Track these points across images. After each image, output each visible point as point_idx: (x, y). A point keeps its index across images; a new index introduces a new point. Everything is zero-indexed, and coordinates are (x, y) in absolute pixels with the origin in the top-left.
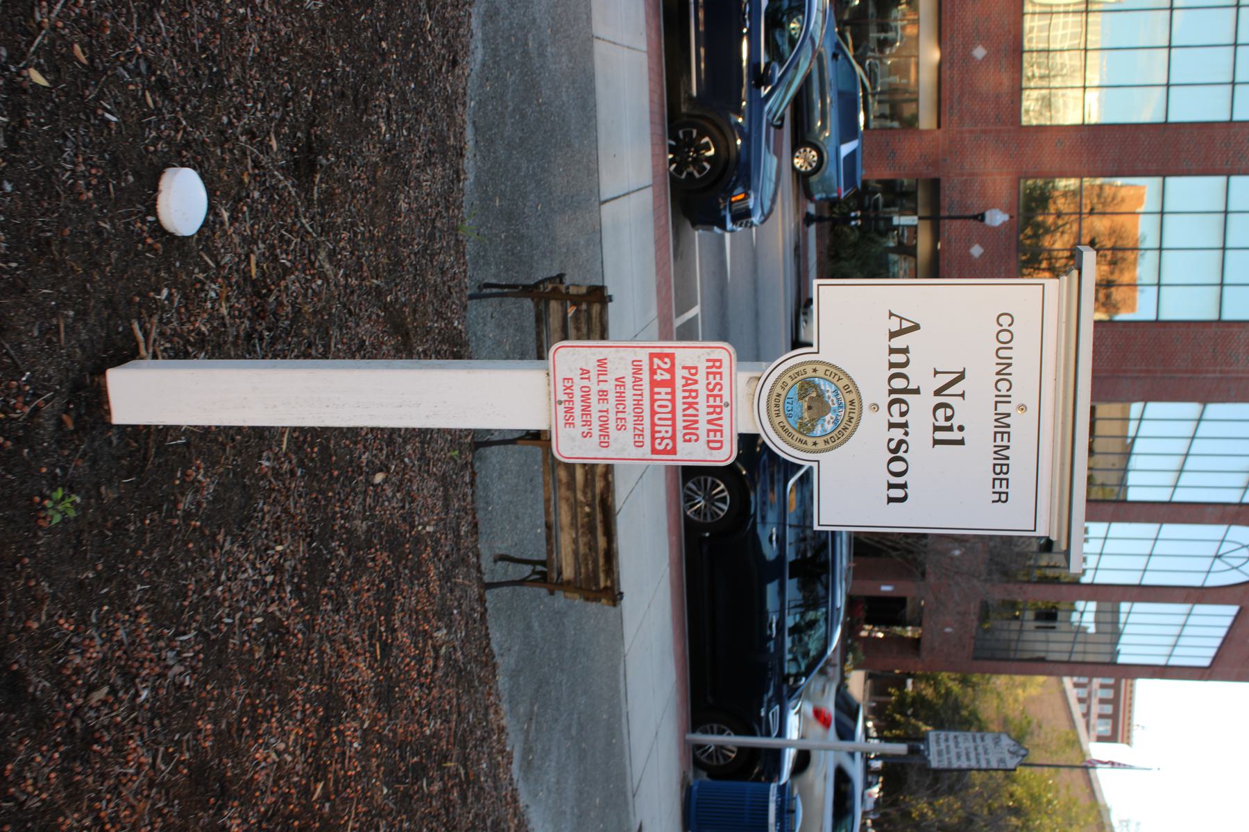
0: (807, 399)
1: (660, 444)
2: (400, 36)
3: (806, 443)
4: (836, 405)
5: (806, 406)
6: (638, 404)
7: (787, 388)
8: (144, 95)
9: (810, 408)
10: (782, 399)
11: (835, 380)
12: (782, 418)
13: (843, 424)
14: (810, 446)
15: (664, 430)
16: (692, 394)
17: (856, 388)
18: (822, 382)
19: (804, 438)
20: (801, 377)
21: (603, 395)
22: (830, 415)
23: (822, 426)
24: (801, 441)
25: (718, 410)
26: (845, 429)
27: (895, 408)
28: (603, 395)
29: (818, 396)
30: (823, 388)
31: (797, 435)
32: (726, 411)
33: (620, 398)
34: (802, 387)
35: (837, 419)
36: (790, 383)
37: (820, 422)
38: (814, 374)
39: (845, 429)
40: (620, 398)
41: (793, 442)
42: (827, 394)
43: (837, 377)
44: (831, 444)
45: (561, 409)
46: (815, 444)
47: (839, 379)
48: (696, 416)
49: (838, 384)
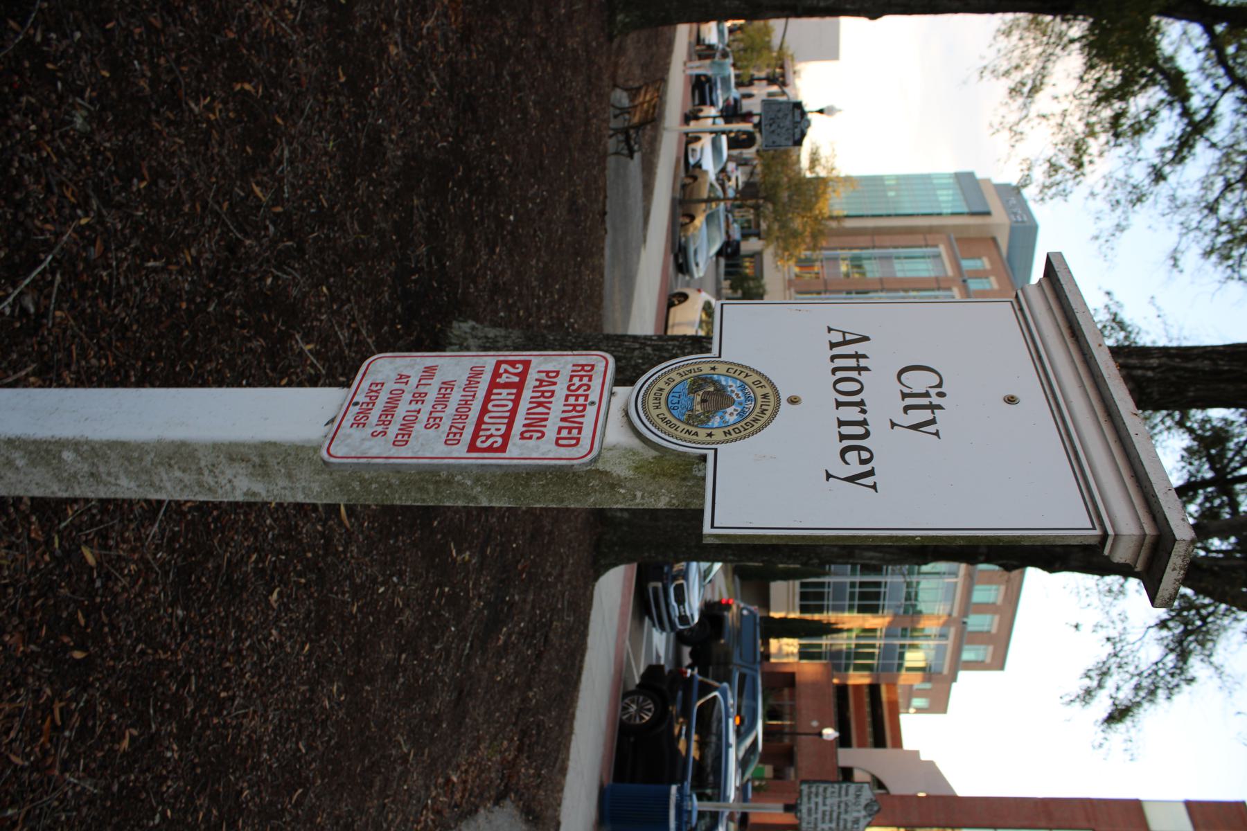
0: (701, 393)
1: (483, 442)
2: (400, 518)
3: (696, 434)
4: (742, 398)
5: (699, 399)
6: (466, 403)
7: (673, 384)
8: (41, 627)
9: (703, 401)
10: (665, 393)
11: (736, 375)
12: (663, 409)
13: (753, 415)
14: (673, 375)
15: (495, 430)
16: (542, 402)
17: (768, 380)
18: (722, 379)
19: (694, 430)
20: (693, 374)
21: (419, 397)
22: (733, 407)
23: (722, 418)
24: (689, 432)
25: (580, 408)
26: (755, 420)
27: (852, 456)
28: (419, 397)
29: (717, 390)
30: (724, 383)
31: (682, 426)
32: (591, 411)
33: (443, 400)
34: (694, 382)
35: (743, 411)
36: (678, 379)
37: (720, 414)
38: (712, 372)
39: (755, 420)
40: (443, 400)
41: (678, 433)
42: (729, 389)
43: (738, 372)
44: (734, 435)
45: (354, 410)
46: (710, 435)
47: (747, 376)
48: (548, 414)
49: (746, 380)
